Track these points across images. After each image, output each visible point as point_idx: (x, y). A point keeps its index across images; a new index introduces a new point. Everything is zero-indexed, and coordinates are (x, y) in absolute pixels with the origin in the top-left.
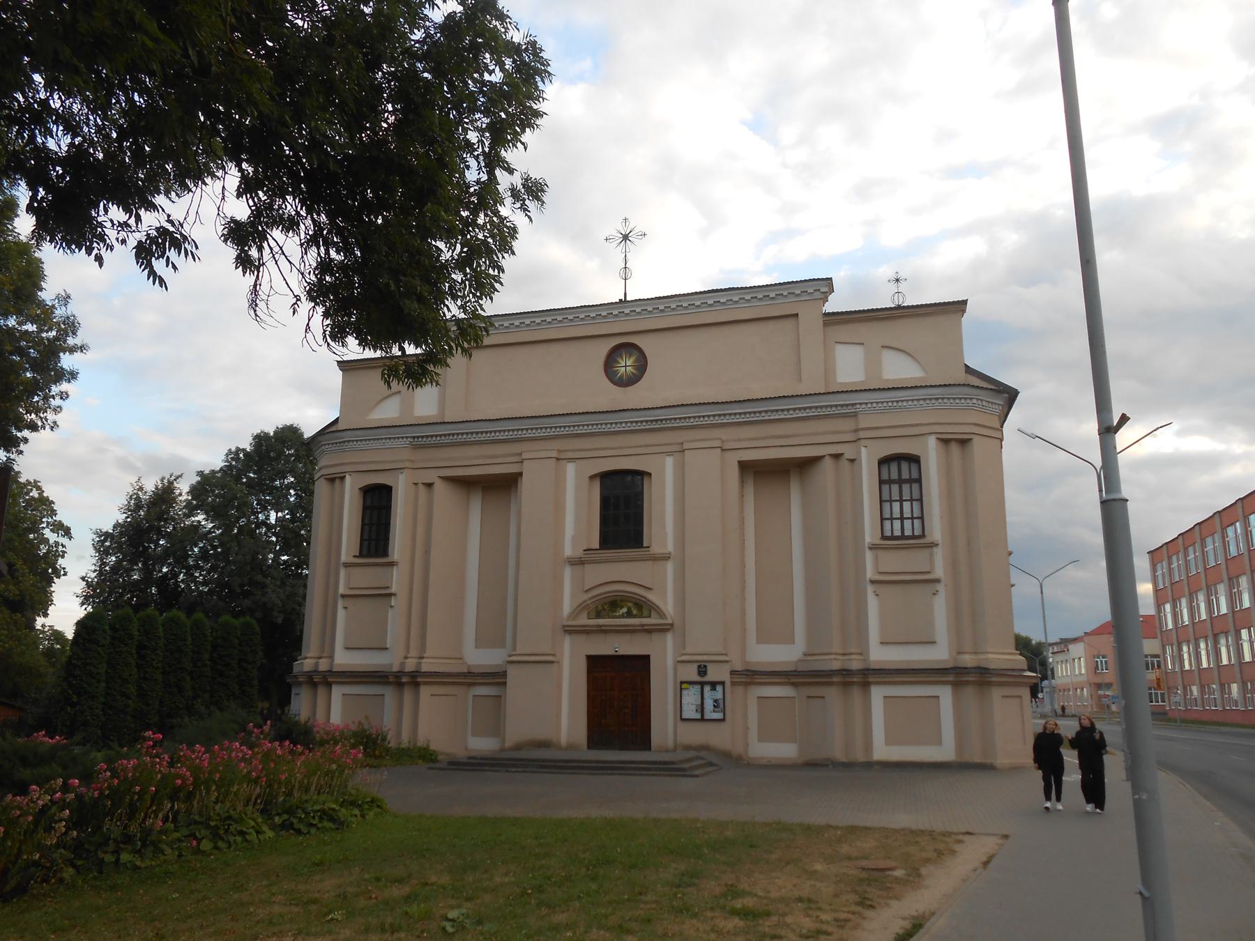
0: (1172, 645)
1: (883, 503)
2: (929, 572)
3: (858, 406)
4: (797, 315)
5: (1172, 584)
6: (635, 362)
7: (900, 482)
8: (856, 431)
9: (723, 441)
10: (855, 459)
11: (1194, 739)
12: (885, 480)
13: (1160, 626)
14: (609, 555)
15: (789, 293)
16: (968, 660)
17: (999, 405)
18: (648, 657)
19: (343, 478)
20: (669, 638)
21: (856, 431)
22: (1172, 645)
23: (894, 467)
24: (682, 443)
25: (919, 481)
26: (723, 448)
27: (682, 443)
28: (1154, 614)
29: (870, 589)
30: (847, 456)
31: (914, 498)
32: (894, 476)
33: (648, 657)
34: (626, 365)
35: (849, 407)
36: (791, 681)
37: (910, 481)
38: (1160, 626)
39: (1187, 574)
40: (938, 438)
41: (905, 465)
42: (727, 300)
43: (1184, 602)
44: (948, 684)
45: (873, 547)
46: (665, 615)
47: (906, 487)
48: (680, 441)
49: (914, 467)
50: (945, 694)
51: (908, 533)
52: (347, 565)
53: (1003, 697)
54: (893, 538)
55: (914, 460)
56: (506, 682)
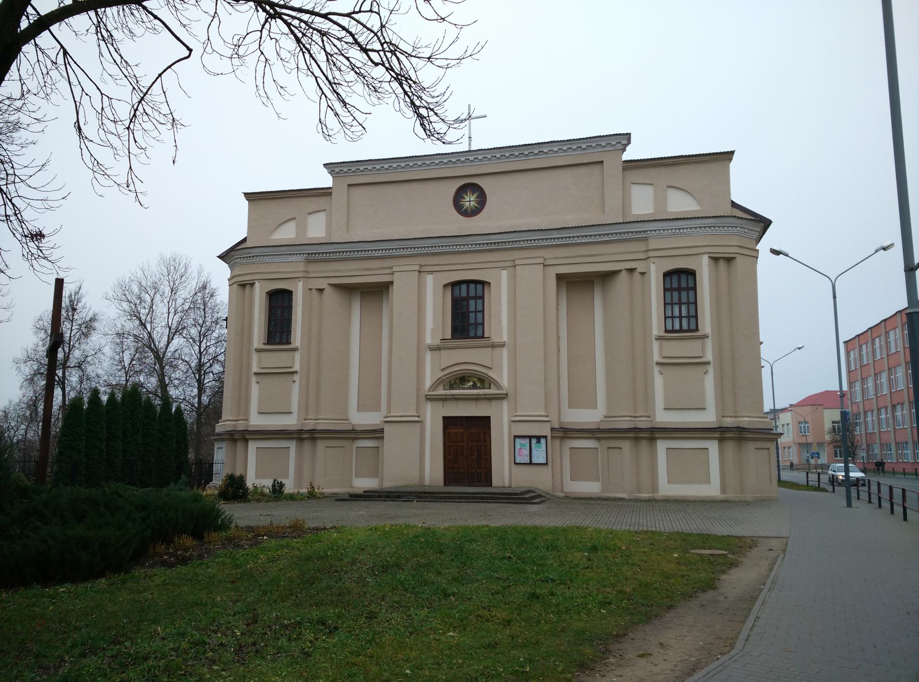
1: (694, 315)
3: (649, 232)
4: (602, 162)
6: (477, 198)
8: (647, 251)
9: (545, 259)
10: (646, 273)
16: (729, 422)
17: (756, 231)
18: (489, 418)
19: (252, 284)
20: (505, 404)
21: (647, 251)
23: (675, 279)
24: (514, 260)
27: (514, 260)
29: (254, 379)
30: (640, 270)
33: (489, 418)
34: (470, 200)
37: (688, 289)
40: (709, 257)
41: (683, 277)
45: (659, 338)
50: (713, 447)
51: (685, 326)
52: (258, 351)
53: (756, 449)
55: (691, 273)
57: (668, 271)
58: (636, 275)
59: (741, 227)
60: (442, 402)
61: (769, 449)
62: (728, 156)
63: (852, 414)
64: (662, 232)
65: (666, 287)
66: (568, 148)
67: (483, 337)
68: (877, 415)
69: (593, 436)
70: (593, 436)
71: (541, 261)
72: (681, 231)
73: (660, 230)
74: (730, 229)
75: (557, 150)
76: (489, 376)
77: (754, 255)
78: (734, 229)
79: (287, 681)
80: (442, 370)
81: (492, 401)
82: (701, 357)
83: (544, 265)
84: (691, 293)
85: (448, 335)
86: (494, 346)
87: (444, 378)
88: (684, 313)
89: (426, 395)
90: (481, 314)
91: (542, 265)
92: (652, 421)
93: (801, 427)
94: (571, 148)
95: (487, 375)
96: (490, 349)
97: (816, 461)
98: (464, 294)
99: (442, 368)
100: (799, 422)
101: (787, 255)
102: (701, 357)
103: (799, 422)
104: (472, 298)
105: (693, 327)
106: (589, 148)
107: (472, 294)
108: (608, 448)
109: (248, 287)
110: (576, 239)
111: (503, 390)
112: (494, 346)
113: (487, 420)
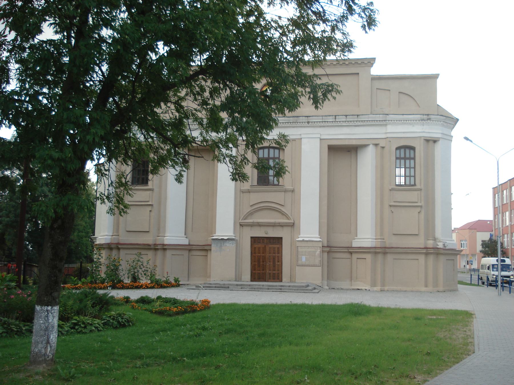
0: (508, 234)
1: (413, 175)
2: (417, 202)
3: (388, 121)
4: (358, 74)
5: (502, 205)
7: (405, 159)
9: (321, 135)
10: (384, 147)
11: (289, 286)
12: (403, 159)
13: (495, 225)
14: (272, 188)
15: (355, 63)
17: (452, 124)
18: (282, 238)
22: (508, 234)
23: (402, 151)
24: (301, 135)
25: (414, 159)
26: (321, 138)
27: (301, 135)
28: (492, 220)
31: (411, 167)
32: (402, 155)
33: (282, 238)
35: (383, 122)
36: (349, 251)
37: (410, 159)
38: (495, 225)
39: (510, 200)
41: (407, 151)
42: (331, 64)
43: (507, 213)
44: (423, 254)
46: (290, 218)
47: (408, 162)
48: (299, 133)
49: (412, 152)
51: (408, 183)
53: (447, 260)
54: (400, 185)
55: (413, 148)
56: (211, 249)
57: (410, 146)
58: (379, 147)
59: (443, 122)
60: (250, 227)
61: (454, 260)
62: (435, 77)
63: (495, 236)
64: (395, 121)
65: (397, 157)
66: (343, 63)
67: (278, 185)
68: (510, 237)
69: (347, 251)
70: (347, 251)
71: (319, 136)
72: (407, 122)
73: (394, 120)
74: (437, 122)
75: (329, 64)
76: (282, 211)
77: (449, 138)
78: (439, 122)
79: (3, 279)
80: (251, 206)
81: (284, 227)
82: (417, 202)
83: (320, 139)
84: (412, 162)
85: (255, 183)
86: (286, 191)
87: (252, 211)
88: (408, 174)
89: (240, 223)
90: (407, 175)
91: (319, 139)
92: (385, 242)
93: (462, 244)
94: (345, 63)
95: (281, 210)
96: (283, 193)
97: (470, 267)
98: (266, 156)
99: (251, 205)
100: (461, 240)
101: (472, 141)
102: (417, 202)
103: (461, 240)
104: (271, 158)
105: (412, 183)
106: (350, 64)
107: (271, 155)
108: (357, 258)
109: (431, 143)
110: (355, 122)
111: (291, 220)
112: (286, 191)
113: (279, 240)
